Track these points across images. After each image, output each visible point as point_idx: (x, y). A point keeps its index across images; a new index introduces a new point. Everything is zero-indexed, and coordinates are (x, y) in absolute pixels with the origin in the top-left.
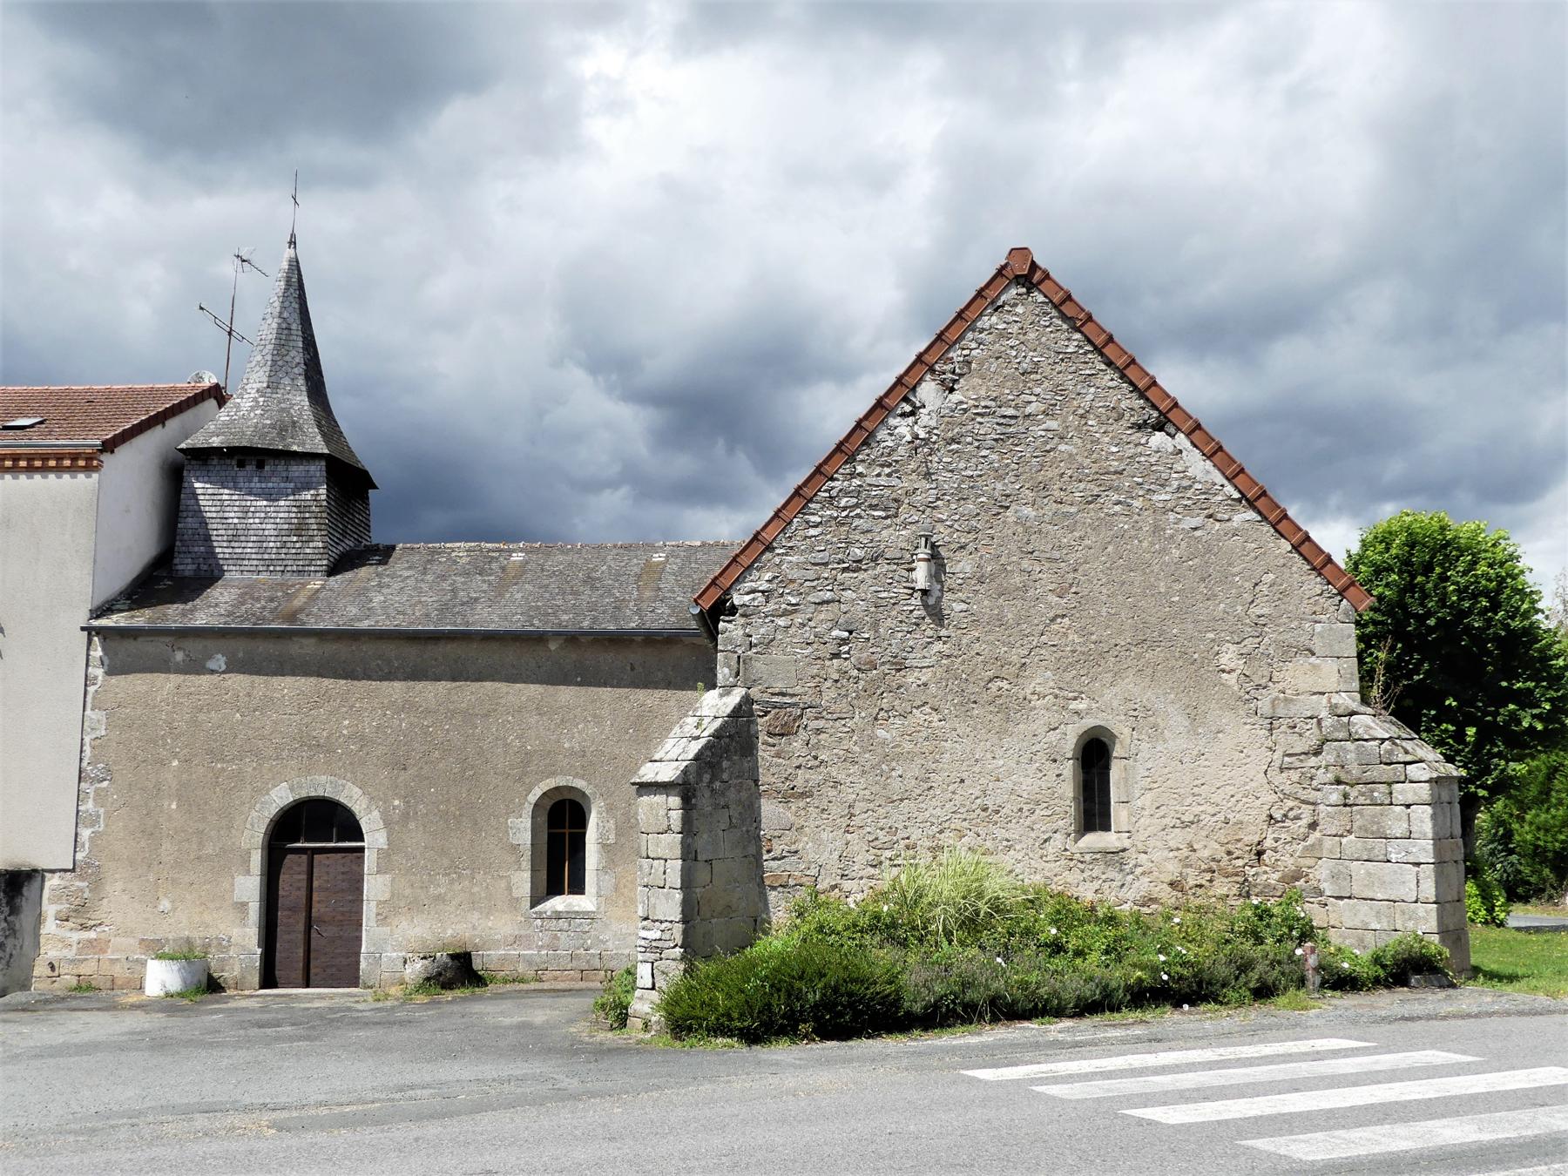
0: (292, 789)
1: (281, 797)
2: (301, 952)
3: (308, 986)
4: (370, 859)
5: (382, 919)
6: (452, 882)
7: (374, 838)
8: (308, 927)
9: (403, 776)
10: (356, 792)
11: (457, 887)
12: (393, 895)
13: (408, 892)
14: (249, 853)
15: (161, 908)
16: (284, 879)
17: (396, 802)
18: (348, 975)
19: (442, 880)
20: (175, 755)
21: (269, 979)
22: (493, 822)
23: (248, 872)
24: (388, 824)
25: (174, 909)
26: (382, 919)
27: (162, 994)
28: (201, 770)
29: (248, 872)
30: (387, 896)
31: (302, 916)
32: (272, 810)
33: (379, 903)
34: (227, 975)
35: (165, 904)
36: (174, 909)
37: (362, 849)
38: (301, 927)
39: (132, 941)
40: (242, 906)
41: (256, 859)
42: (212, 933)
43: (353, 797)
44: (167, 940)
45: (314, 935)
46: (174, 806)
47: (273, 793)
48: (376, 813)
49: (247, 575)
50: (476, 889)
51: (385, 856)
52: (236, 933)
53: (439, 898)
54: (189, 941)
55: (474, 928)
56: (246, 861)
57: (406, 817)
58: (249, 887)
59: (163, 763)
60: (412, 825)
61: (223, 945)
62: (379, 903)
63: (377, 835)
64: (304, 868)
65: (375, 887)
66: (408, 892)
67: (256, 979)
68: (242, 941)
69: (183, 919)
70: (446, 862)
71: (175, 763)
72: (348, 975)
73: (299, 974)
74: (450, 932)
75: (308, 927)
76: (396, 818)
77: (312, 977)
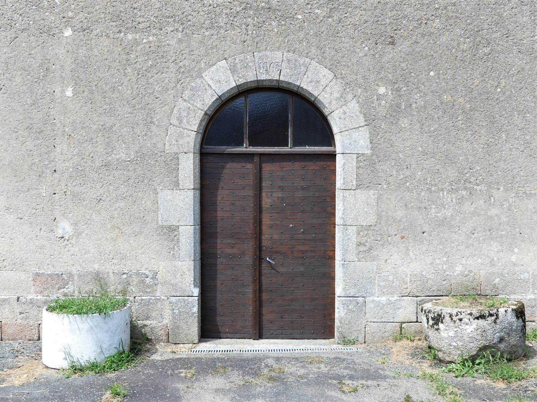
0: (233, 70)
1: (219, 81)
2: (249, 291)
3: (260, 336)
4: (344, 170)
5: (365, 250)
6: (461, 201)
7: (350, 138)
8: (259, 259)
9: (391, 54)
10: (325, 74)
11: (468, 207)
12: (379, 217)
13: (400, 213)
14: (176, 157)
15: (60, 232)
16: (223, 196)
17: (382, 90)
18: (319, 322)
19: (447, 198)
20: (68, 22)
21: (208, 331)
22: (517, 119)
23: (176, 185)
24: (370, 121)
25: (78, 234)
26: (365, 250)
27: (65, 365)
28: (105, 42)
29: (176, 185)
30: (371, 219)
31: (249, 246)
32: (207, 100)
33: (361, 229)
34: (155, 324)
35: (65, 227)
36: (78, 234)
37: (332, 156)
38: (249, 259)
39: (23, 276)
40: (171, 231)
41: (188, 167)
42: (130, 266)
43: (319, 82)
44: (71, 275)
45: (265, 270)
46: (69, 93)
47: (208, 76)
48: (353, 105)
49: (44, 297)
50: (493, 212)
51: (368, 164)
52: (162, 267)
53: (443, 222)
54: (99, 278)
55: (492, 263)
56: (172, 164)
57: (396, 111)
58: (180, 204)
59: (49, 32)
60: (404, 123)
61: (148, 282)
62: (361, 229)
63: (356, 135)
64: (250, 180)
65: (351, 207)
66: (400, 213)
67: (194, 329)
68: (170, 279)
69: (90, 249)
70: (452, 173)
71: (68, 33)
72: (319, 322)
73: (249, 321)
74: (459, 269)
75: (259, 259)
76: (383, 112)
77: (266, 325)
